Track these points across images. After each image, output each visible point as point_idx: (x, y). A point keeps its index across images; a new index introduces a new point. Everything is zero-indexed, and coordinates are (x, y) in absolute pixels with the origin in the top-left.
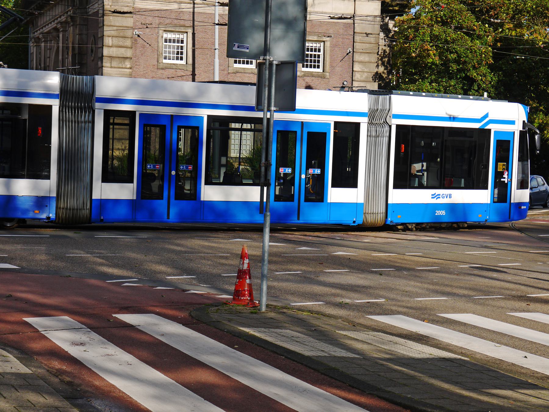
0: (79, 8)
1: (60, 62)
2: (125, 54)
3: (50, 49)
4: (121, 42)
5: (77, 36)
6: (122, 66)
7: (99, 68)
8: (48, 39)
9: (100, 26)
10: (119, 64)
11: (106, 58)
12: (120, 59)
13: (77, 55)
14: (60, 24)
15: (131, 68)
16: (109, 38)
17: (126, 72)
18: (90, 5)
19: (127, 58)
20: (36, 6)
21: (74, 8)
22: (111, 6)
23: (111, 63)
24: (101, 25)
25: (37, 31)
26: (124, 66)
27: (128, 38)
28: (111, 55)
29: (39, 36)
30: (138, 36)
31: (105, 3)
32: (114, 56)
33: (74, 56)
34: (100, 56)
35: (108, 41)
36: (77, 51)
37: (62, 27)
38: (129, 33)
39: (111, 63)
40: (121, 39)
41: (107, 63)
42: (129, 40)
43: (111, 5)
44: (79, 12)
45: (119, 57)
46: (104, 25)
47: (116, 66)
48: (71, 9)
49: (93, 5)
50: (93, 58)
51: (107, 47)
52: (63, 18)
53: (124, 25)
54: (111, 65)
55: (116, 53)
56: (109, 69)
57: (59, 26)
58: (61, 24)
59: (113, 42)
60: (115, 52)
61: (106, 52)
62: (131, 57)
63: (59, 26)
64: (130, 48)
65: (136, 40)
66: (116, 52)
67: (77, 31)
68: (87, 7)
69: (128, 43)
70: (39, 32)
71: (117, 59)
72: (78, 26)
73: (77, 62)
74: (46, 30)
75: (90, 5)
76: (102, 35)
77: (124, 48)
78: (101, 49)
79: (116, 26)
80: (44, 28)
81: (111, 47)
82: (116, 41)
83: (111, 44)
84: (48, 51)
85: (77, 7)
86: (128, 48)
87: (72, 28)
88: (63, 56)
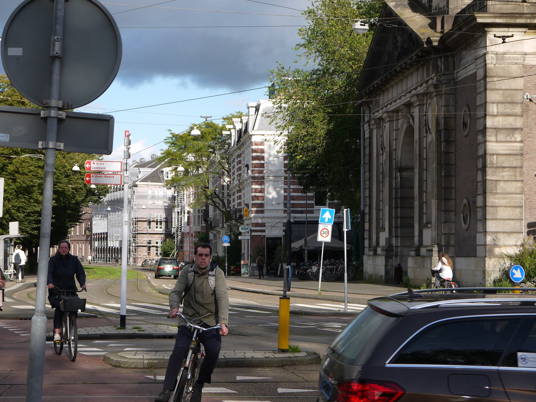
0: (444, 74)
1: (416, 142)
2: (514, 124)
3: (397, 130)
4: (508, 109)
5: (443, 108)
6: (511, 139)
7: (480, 144)
8: (393, 118)
9: (478, 91)
10: (507, 137)
11: (491, 130)
12: (508, 130)
13: (443, 132)
14: (433, 86)
15: (521, 142)
16: (494, 105)
17: (517, 147)
18: (460, 69)
19: (516, 129)
20: (381, 80)
21: (438, 74)
22: (495, 65)
23: (496, 136)
24: (482, 89)
25: (378, 111)
26: (513, 139)
27: (517, 103)
28: (496, 126)
29: (382, 116)
30: (531, 100)
31: (488, 62)
32: (500, 127)
33: (438, 132)
34: (481, 128)
35: (492, 109)
36: (442, 126)
37: (389, 117)
38: (518, 98)
39: (496, 136)
40: (508, 106)
41: (491, 136)
42: (519, 105)
43: (495, 63)
44: (445, 79)
45: (506, 129)
46: (486, 89)
47: (503, 140)
48: (434, 76)
49: (465, 67)
50: (466, 133)
51: (491, 117)
52: (420, 90)
53: (512, 87)
54: (497, 139)
55: (503, 123)
56: (495, 144)
57: (414, 99)
58: (417, 97)
59: (498, 110)
60: (501, 123)
61: (490, 122)
62: (522, 127)
63: (414, 99)
64: (520, 116)
65: (527, 106)
66: (502, 122)
67: (443, 103)
68: (456, 72)
69: (518, 109)
70: (381, 111)
71: (504, 131)
72: (443, 96)
73: (443, 139)
74: (391, 108)
75: (460, 69)
76: (484, 102)
77: (512, 117)
78: (482, 120)
79: (502, 90)
80: (389, 106)
81: (496, 116)
82: (502, 108)
83: (496, 112)
84: (394, 131)
85: (442, 73)
86: (517, 116)
87: (435, 99)
88: (420, 134)
